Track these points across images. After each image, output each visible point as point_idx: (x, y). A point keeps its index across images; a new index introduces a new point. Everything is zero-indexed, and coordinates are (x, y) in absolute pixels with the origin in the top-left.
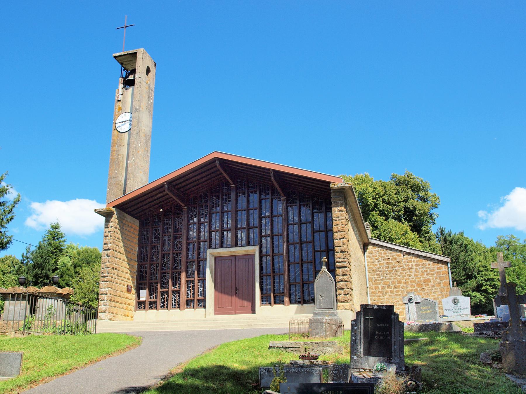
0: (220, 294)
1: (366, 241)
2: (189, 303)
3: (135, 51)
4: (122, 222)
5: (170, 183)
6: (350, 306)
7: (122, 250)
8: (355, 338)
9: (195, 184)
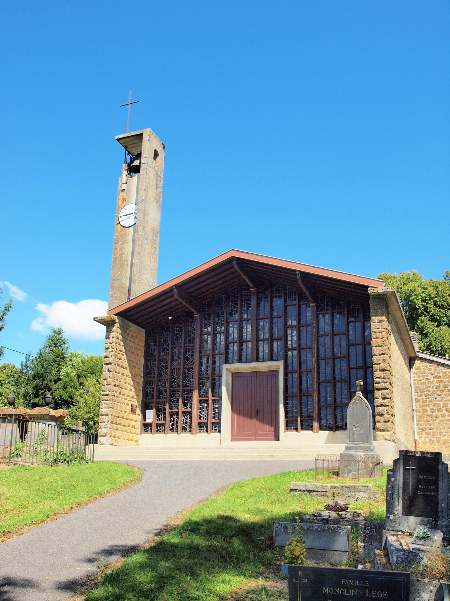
0: (238, 416)
1: (413, 355)
2: (202, 426)
3: (141, 132)
4: (125, 332)
5: (179, 286)
6: (391, 436)
7: (126, 364)
8: (392, 492)
9: (213, 285)
